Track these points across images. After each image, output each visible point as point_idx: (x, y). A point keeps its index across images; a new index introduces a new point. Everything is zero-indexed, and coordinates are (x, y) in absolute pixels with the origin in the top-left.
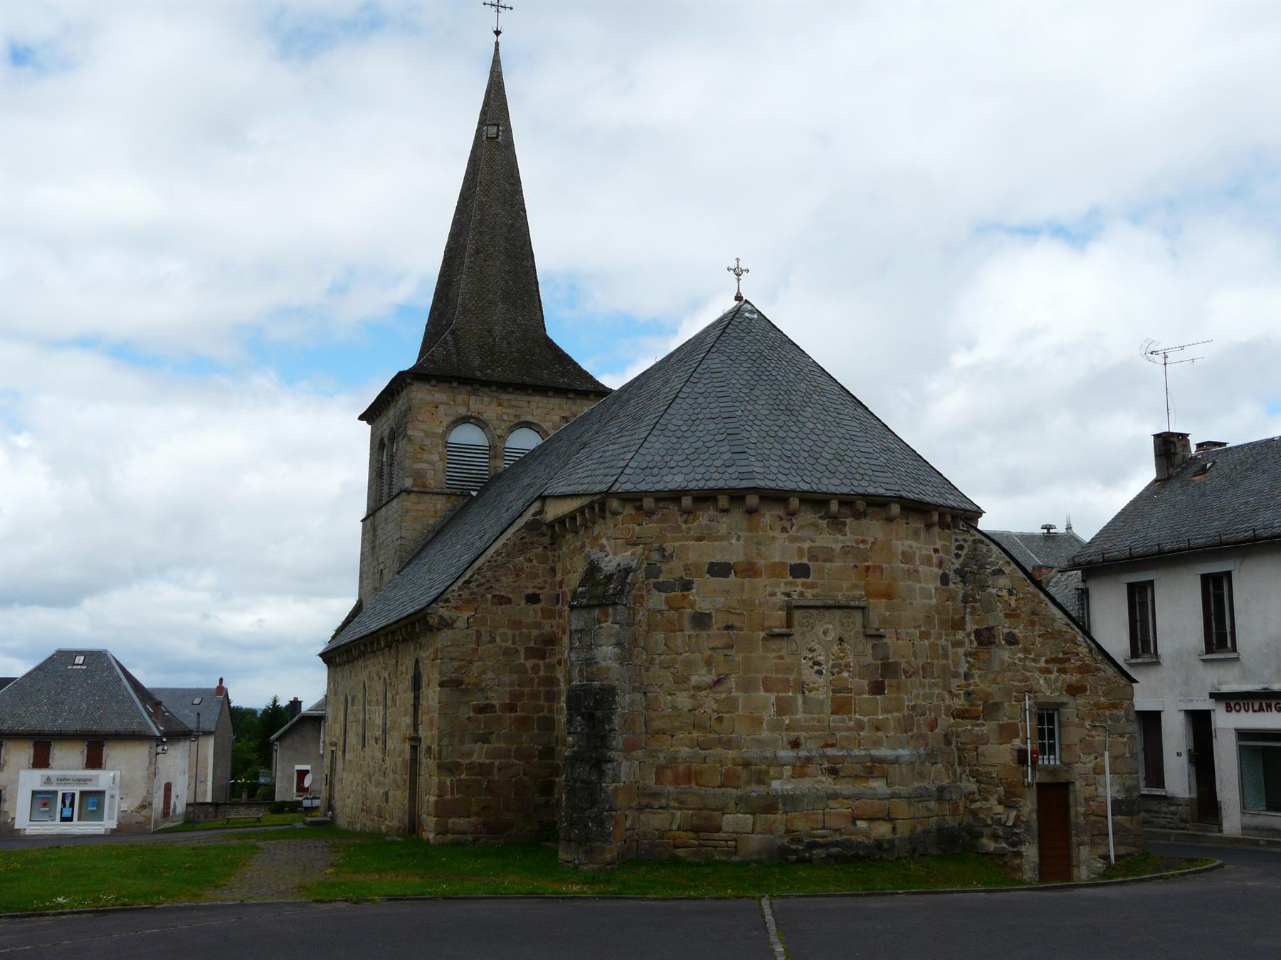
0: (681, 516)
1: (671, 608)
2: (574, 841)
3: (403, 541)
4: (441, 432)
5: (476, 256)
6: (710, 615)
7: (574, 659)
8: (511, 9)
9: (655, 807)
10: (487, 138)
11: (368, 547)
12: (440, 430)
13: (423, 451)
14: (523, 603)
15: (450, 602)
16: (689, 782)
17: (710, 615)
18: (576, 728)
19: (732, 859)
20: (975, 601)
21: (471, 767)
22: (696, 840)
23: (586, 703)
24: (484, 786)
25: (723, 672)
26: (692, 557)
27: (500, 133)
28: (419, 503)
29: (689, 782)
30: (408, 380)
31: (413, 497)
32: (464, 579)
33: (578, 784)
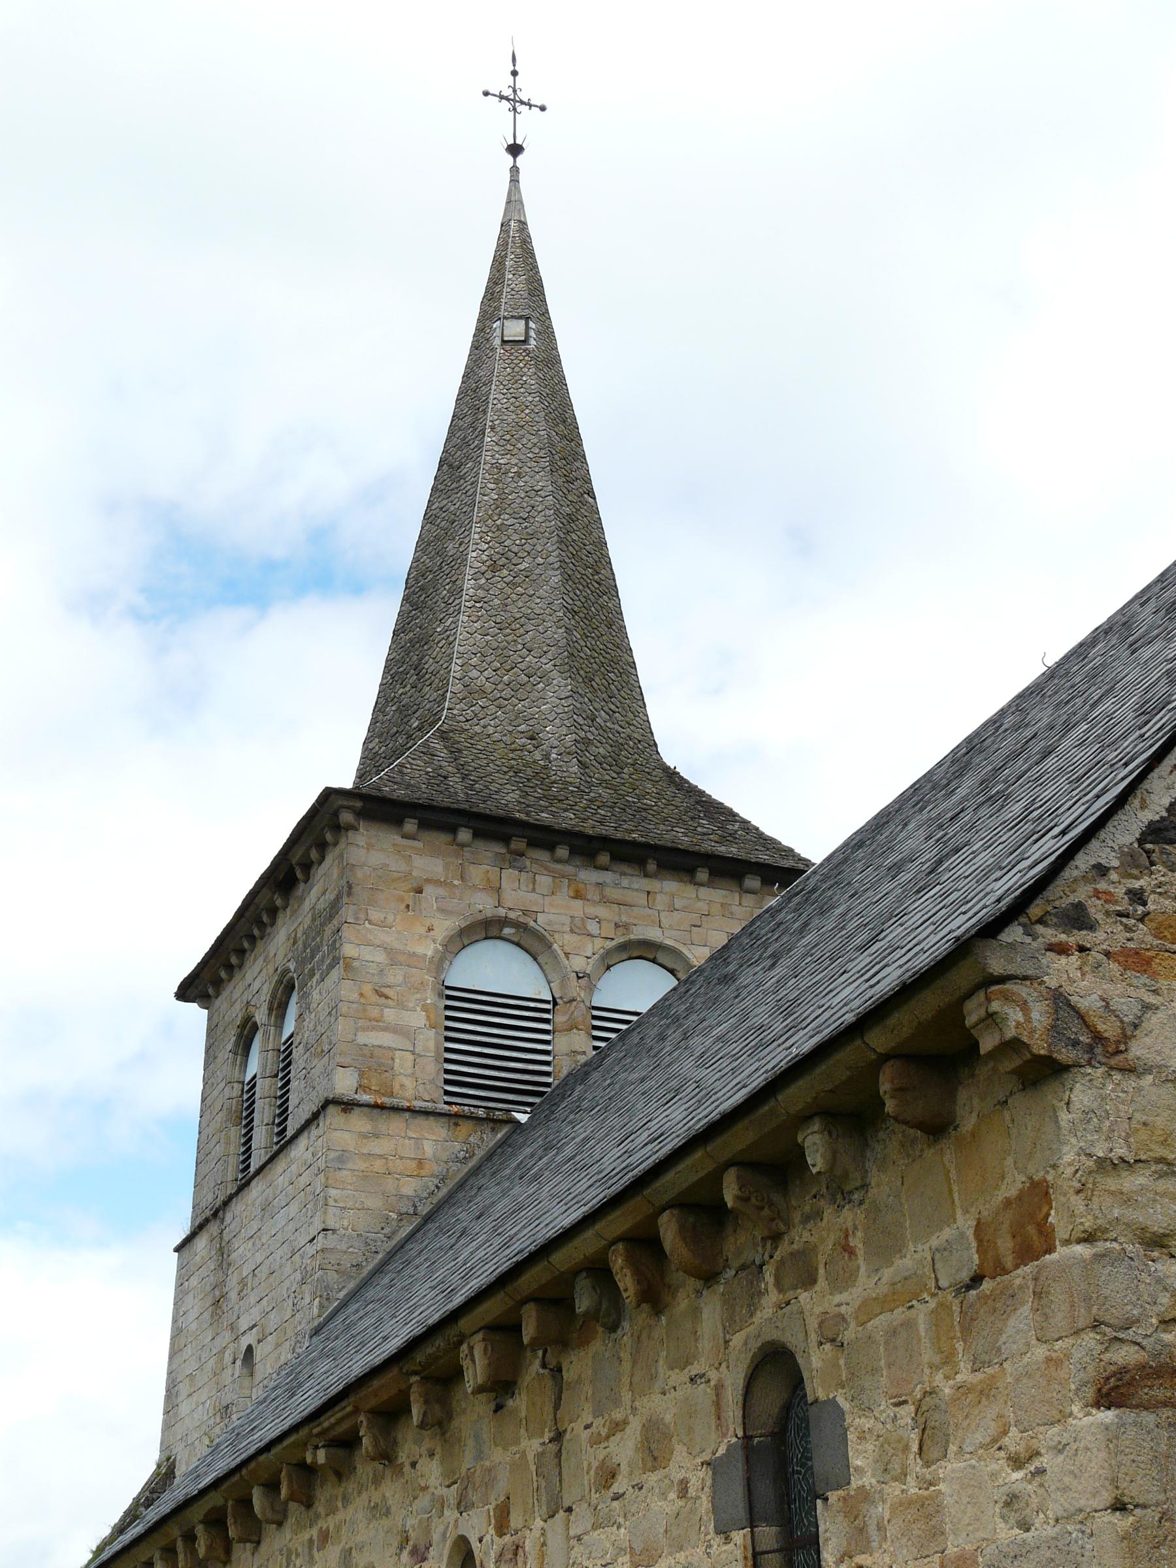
4: (430, 953)
5: (489, 575)
8: (543, 109)
10: (504, 342)
11: (195, 1305)
12: (428, 949)
13: (383, 1000)
15: (1091, 927)
27: (532, 334)
28: (377, 1136)
30: (346, 817)
31: (359, 1122)
32: (1149, 816)
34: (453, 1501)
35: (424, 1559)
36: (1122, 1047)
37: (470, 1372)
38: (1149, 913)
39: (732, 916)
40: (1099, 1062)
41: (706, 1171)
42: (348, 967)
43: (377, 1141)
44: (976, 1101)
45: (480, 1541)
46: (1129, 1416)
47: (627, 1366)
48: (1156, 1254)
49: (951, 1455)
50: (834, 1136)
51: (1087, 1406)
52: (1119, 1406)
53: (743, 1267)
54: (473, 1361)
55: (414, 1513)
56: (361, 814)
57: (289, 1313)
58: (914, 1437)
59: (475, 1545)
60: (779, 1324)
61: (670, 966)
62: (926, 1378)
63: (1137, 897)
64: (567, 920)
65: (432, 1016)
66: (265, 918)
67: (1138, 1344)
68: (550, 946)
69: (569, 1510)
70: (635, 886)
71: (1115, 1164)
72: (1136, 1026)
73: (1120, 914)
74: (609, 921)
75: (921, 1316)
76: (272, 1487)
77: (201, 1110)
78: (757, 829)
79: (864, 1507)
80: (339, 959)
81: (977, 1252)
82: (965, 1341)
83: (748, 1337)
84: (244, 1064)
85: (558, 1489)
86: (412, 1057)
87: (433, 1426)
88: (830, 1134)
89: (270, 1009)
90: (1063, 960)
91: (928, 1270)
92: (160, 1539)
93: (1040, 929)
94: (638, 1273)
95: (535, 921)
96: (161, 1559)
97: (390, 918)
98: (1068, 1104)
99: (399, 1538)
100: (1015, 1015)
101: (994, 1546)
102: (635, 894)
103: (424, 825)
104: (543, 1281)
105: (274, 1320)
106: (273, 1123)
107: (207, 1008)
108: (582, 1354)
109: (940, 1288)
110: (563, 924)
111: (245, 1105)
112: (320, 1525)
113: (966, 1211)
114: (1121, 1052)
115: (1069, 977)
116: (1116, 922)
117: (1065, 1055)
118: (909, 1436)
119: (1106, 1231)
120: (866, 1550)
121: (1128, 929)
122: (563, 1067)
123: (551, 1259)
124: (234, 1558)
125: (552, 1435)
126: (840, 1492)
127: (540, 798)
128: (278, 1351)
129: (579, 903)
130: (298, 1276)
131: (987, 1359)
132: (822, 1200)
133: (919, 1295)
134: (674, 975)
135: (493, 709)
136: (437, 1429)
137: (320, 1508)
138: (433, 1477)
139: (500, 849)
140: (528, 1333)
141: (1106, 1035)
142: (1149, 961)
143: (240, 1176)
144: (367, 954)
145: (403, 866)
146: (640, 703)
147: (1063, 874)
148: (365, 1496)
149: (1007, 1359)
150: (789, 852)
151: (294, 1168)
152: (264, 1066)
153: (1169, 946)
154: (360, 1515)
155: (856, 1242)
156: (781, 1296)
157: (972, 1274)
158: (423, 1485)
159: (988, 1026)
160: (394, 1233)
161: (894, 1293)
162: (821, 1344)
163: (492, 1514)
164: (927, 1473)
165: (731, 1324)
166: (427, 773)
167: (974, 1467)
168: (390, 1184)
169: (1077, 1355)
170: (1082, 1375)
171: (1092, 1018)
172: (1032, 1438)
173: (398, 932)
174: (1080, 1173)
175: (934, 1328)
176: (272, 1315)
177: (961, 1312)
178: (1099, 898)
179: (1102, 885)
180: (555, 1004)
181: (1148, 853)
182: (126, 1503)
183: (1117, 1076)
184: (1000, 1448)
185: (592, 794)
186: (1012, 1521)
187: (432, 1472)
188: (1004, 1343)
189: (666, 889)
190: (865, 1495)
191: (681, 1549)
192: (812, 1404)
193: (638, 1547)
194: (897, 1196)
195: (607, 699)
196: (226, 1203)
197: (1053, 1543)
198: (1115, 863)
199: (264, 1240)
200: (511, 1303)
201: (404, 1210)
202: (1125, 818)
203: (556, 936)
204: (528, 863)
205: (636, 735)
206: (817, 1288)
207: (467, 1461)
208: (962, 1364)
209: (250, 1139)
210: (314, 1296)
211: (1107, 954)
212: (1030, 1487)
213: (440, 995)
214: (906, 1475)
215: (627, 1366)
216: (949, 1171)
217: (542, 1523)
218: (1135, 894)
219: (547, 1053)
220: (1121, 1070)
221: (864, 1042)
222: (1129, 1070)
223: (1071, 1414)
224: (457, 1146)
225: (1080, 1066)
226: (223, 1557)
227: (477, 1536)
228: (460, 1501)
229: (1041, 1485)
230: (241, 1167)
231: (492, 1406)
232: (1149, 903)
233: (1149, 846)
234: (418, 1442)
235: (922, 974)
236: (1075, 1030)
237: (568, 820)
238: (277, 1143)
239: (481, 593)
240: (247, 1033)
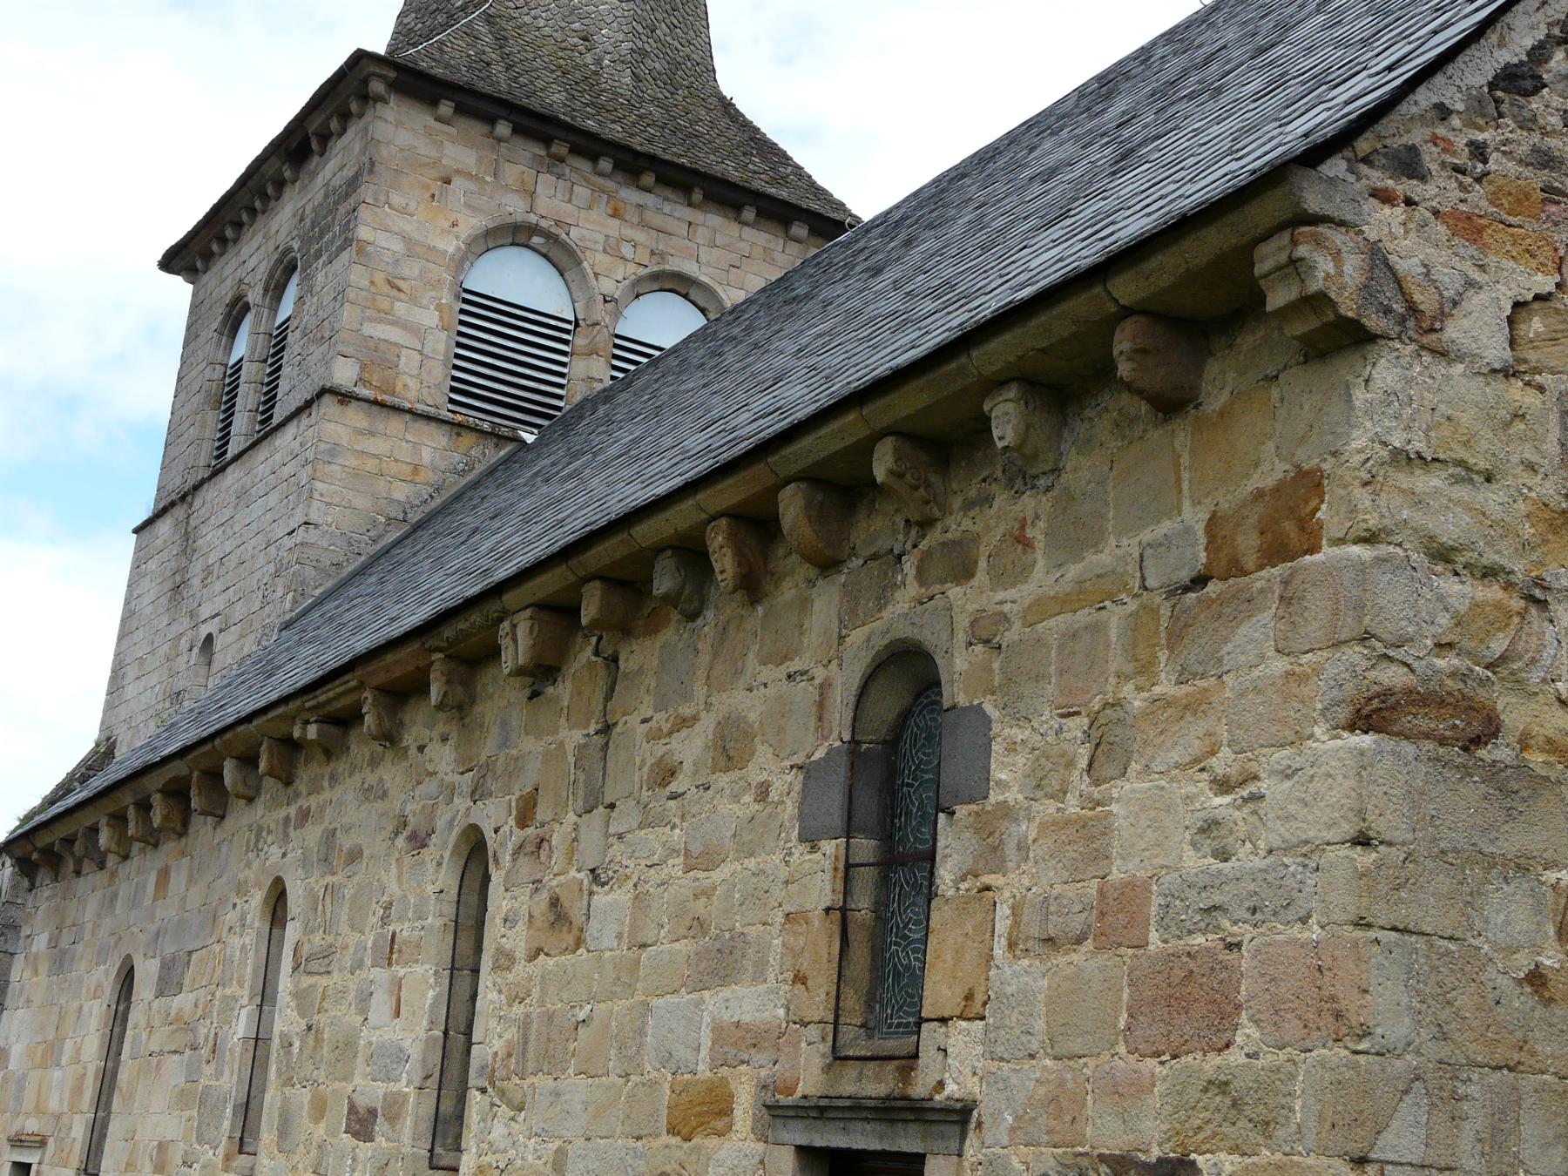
4: (451, 250)
12: (450, 245)
13: (395, 292)
28: (372, 434)
30: (377, 87)
31: (355, 416)
32: (1506, 57)
34: (467, 789)
35: (424, 846)
36: (1437, 325)
37: (510, 651)
38: (1489, 173)
39: (773, 262)
40: (1409, 338)
41: (855, 439)
42: (361, 251)
43: (372, 439)
44: (1231, 376)
45: (496, 831)
46: (1388, 743)
47: (705, 658)
48: (1439, 568)
49: (1131, 772)
50: (1031, 406)
51: (1334, 729)
52: (1378, 731)
53: (875, 557)
54: (515, 641)
55: (417, 798)
56: (394, 86)
57: (257, 605)
58: (1083, 755)
59: (489, 834)
60: (916, 620)
61: (702, 303)
62: (1109, 688)
63: (1479, 151)
64: (601, 239)
65: (446, 317)
66: (270, 191)
67: (1408, 666)
68: (579, 263)
69: (612, 806)
70: (677, 214)
71: (1410, 459)
72: (1455, 304)
73: (1458, 170)
74: (645, 247)
75: (1114, 622)
76: (248, 760)
77: (176, 390)
78: (810, 177)
79: (1003, 825)
80: (352, 240)
81: (1206, 549)
82: (1171, 649)
83: (872, 632)
84: (229, 348)
85: (600, 783)
86: (419, 357)
87: (453, 708)
88: (1026, 404)
89: (266, 290)
90: (1387, 210)
91: (1132, 568)
92: (110, 806)
93: (1364, 169)
94: (740, 554)
95: (568, 234)
96: (108, 825)
97: (413, 206)
98: (1367, 381)
99: (396, 823)
100: (1325, 265)
101: (1176, 875)
102: (676, 222)
103: (461, 110)
104: (618, 556)
105: (239, 611)
106: (257, 410)
107: (192, 283)
108: (648, 643)
109: (1146, 589)
110: (596, 242)
111: (226, 389)
112: (299, 804)
113: (1196, 502)
114: (1436, 331)
115: (1390, 232)
116: (1450, 177)
117: (1374, 322)
118: (1075, 751)
119: (1390, 533)
120: (1000, 868)
121: (1462, 187)
122: (576, 392)
123: (633, 532)
124: (191, 830)
125: (599, 727)
126: (974, 807)
127: (587, 105)
128: (241, 642)
129: (616, 222)
130: (272, 568)
131: (1200, 670)
132: (994, 485)
133: (1115, 595)
134: (705, 315)
136: (455, 712)
137: (301, 785)
138: (444, 764)
140: (588, 614)
141: (1422, 307)
142: (1480, 231)
143: (213, 463)
144: (383, 239)
145: (434, 153)
146: (704, 23)
147: (1398, 108)
148: (357, 776)
149: (1229, 671)
150: (840, 206)
151: (278, 457)
152: (253, 349)
153: (1505, 216)
154: (350, 796)
155: (1036, 533)
156: (923, 590)
157: (1194, 574)
158: (431, 770)
159: (1286, 276)
160: (380, 536)
161: (1080, 593)
162: (971, 644)
163: (514, 804)
165: (850, 617)
166: (469, 56)
167: (1163, 788)
168: (381, 486)
169: (1331, 671)
170: (1335, 692)
171: (1410, 285)
172: (1250, 760)
173: (420, 223)
174: (1371, 462)
175: (1130, 633)
176: (238, 606)
177: (1171, 617)
178: (1436, 145)
179: (1441, 131)
180: (577, 325)
181: (1498, 101)
182: (59, 776)
183: (1427, 358)
184: (1202, 770)
185: (642, 110)
186: (1206, 849)
187: (443, 758)
188: (1229, 653)
189: (709, 223)
190: (1006, 812)
191: (752, 854)
192: (948, 710)
193: (696, 848)
194: (1102, 483)
195: (670, 11)
196: (196, 488)
197: (1260, 876)
198: (1460, 106)
199: (236, 529)
200: (572, 578)
201: (393, 515)
202: (1478, 54)
203: (588, 253)
204: (567, 171)
205: (695, 56)
206: (974, 582)
207: (488, 749)
208: (1163, 675)
209: (230, 424)
210: (288, 589)
211: (1436, 213)
212: (1237, 813)
213: (457, 297)
214: (1065, 793)
215: (705, 658)
216: (1180, 456)
217: (575, 818)
218: (1477, 148)
219: (562, 375)
220: (1433, 351)
221: (1106, 290)
222: (1441, 353)
223: (1311, 736)
224: (457, 457)
225: (1390, 339)
226: (179, 828)
227: (493, 826)
228: (476, 789)
229: (1254, 812)
230: (215, 453)
231: (527, 692)
232: (1491, 162)
233: (1499, 94)
234: (430, 725)
235: (1213, 204)
236: (1389, 294)
237: (615, 132)
238: (259, 432)
240: (236, 312)
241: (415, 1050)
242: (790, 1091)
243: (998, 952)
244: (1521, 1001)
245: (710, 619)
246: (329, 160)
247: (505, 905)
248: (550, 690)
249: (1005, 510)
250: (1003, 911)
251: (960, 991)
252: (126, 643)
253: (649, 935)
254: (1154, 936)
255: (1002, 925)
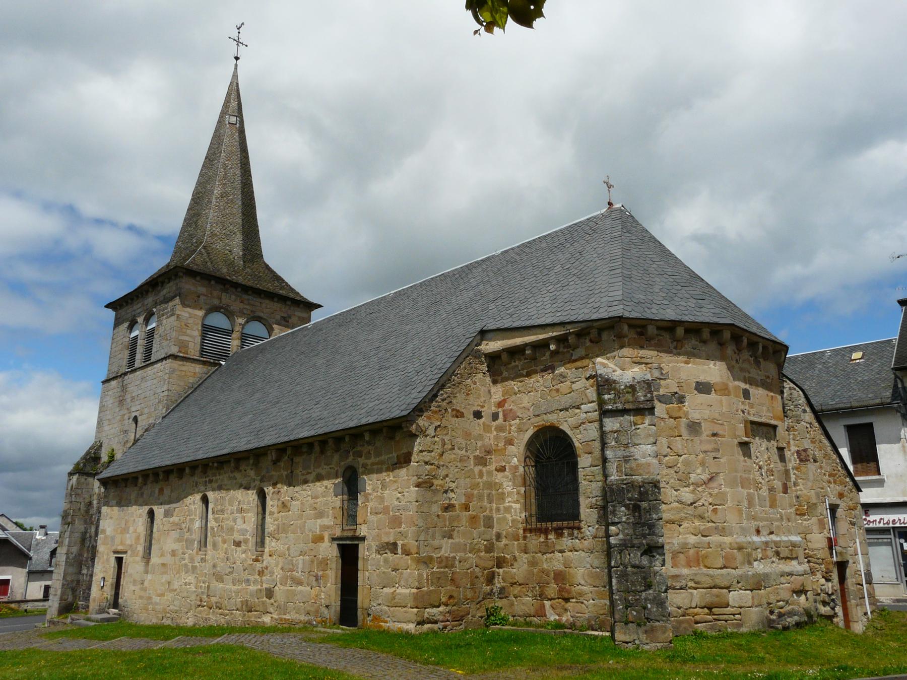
0: (672, 343)
1: (671, 417)
2: (632, 622)
3: (170, 393)
4: (201, 315)
6: (700, 423)
7: (611, 456)
8: (246, 46)
9: (676, 588)
10: (229, 123)
14: (472, 416)
16: (699, 565)
17: (700, 423)
18: (620, 518)
19: (741, 630)
20: (795, 430)
21: (440, 560)
22: (709, 615)
23: (630, 495)
24: (450, 578)
25: (715, 471)
26: (683, 376)
29: (699, 565)
33: (629, 569)
105: (146, 411)
117: (417, 433)
120: (368, 502)
129: (242, 304)
130: (157, 401)
135: (219, 241)
139: (222, 287)
151: (155, 370)
164: (382, 492)
187: (252, 473)
193: (313, 495)
219: (229, 345)
239: (217, 204)
241: (250, 530)
242: (335, 535)
243: (369, 514)
244: (436, 519)
245: (313, 456)
246: (164, 289)
247: (271, 503)
248: (278, 463)
249: (366, 449)
250: (369, 509)
251: (363, 520)
252: (101, 415)
253: (305, 509)
254: (391, 513)
255: (369, 510)
